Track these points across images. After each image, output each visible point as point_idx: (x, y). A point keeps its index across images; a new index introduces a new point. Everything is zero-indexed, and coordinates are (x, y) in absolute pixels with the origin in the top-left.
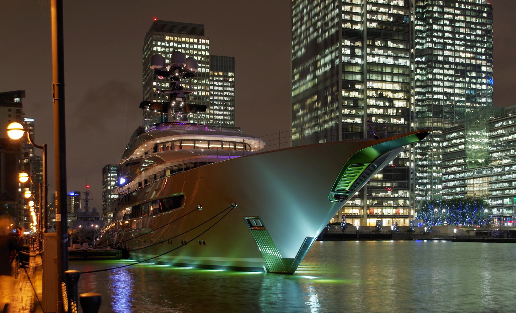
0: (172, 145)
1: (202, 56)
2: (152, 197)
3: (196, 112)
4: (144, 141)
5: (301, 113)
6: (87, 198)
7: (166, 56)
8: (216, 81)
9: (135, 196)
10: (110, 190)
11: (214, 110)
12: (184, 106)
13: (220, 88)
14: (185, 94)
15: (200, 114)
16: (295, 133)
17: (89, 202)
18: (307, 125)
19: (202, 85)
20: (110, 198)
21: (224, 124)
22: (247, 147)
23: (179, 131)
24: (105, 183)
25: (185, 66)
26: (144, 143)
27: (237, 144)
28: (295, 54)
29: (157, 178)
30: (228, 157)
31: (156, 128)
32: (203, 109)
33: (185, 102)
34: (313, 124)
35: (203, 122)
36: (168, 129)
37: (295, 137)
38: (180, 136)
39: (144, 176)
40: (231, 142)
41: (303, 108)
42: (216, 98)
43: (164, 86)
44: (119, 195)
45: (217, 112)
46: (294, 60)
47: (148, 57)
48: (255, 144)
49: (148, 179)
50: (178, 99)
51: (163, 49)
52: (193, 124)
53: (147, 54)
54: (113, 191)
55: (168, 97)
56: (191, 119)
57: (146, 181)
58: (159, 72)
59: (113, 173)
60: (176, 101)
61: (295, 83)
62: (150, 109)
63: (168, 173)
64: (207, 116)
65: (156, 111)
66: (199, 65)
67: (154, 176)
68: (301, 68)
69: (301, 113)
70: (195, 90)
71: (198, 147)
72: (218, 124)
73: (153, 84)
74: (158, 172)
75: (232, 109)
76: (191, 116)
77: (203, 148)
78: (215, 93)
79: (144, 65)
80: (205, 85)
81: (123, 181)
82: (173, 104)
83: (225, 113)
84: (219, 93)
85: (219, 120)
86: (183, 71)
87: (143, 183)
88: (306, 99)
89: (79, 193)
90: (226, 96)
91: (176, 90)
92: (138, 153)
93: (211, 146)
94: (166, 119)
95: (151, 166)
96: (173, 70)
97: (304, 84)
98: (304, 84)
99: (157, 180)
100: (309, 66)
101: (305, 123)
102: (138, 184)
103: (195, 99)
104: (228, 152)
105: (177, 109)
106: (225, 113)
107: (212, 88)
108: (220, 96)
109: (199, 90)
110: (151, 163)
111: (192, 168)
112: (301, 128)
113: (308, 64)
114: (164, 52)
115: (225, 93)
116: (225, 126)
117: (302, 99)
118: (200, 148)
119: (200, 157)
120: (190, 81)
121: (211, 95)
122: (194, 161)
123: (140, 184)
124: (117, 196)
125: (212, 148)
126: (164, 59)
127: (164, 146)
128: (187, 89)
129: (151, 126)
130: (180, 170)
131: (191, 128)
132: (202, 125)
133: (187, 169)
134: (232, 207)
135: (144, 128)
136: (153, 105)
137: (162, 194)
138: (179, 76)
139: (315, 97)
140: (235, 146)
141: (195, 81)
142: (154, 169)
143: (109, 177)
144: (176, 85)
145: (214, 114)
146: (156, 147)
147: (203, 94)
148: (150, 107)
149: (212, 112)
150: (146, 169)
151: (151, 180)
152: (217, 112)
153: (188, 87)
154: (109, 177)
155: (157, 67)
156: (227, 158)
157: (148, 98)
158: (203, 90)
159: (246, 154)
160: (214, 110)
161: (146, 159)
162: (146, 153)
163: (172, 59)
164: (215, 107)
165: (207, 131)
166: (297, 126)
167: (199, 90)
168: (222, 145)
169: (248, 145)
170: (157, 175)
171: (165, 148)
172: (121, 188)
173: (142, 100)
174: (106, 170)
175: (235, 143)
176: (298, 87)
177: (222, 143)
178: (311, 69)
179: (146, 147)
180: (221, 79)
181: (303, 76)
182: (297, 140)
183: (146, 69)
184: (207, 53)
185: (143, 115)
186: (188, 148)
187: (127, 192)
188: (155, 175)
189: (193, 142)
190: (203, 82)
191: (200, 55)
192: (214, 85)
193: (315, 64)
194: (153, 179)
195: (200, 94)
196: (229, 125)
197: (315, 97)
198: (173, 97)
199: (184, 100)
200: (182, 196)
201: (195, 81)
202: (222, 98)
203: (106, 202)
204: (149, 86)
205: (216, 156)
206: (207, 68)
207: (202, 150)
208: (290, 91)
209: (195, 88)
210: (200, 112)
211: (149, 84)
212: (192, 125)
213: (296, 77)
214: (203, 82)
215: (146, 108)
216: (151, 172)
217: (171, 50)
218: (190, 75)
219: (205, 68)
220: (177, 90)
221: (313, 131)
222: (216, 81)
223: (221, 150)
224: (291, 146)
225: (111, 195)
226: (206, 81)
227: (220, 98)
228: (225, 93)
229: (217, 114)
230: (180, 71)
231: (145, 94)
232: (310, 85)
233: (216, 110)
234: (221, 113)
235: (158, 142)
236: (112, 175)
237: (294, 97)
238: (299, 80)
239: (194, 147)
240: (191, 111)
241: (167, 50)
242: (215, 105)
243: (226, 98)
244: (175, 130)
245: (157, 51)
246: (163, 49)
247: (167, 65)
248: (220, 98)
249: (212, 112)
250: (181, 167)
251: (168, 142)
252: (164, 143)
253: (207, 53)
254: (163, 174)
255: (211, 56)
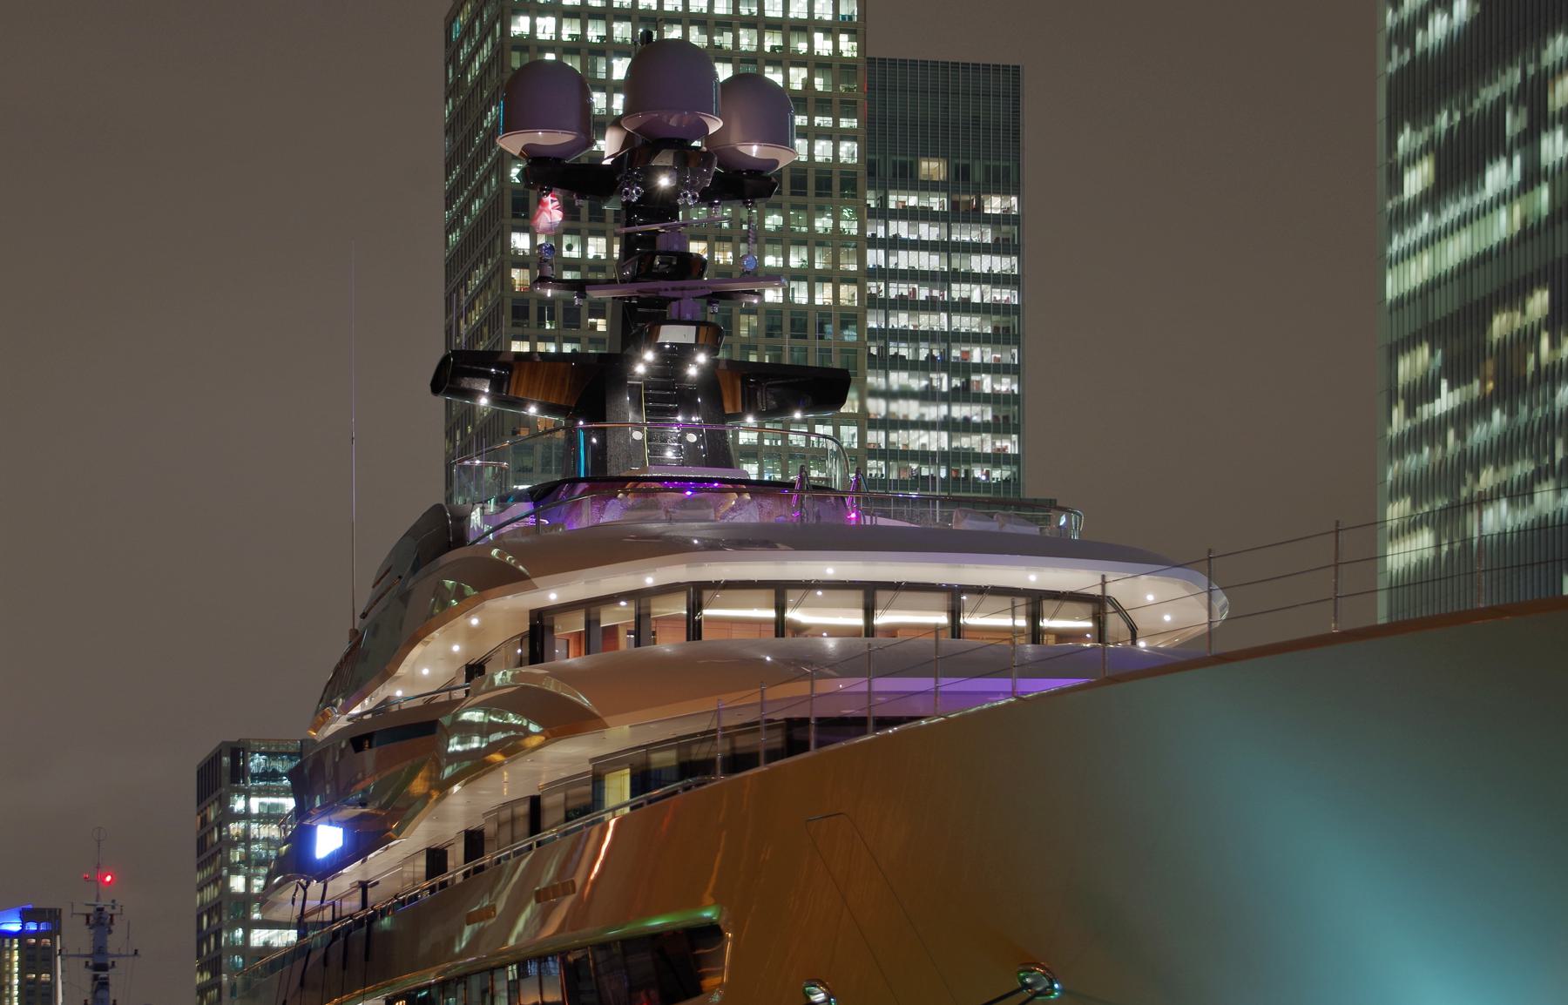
0: (641, 618)
1: (814, 63)
2: (512, 941)
3: (783, 409)
4: (460, 595)
5: (1446, 401)
6: (100, 950)
7: (589, 68)
8: (906, 214)
9: (387, 934)
10: (246, 900)
11: (889, 395)
12: (711, 383)
13: (930, 262)
14: (718, 300)
15: (804, 422)
16: (1411, 526)
17: (113, 976)
18: (1488, 478)
19: (812, 241)
20: (245, 949)
21: (952, 482)
22: (1114, 623)
23: (679, 529)
24: (211, 852)
25: (715, 126)
26: (468, 606)
27: (1048, 606)
28: (1404, 35)
29: (548, 819)
30: (1004, 684)
31: (536, 514)
32: (823, 389)
33: (713, 350)
34: (1523, 468)
35: (835, 473)
36: (607, 518)
37: (1410, 551)
38: (689, 563)
39: (458, 809)
40: (998, 590)
41: (1457, 372)
42: (901, 320)
43: (575, 253)
44: (301, 925)
45: (910, 409)
46: (1401, 70)
47: (480, 81)
48: (1164, 607)
49: (490, 829)
50: (671, 335)
51: (570, 29)
52: (760, 483)
53: (471, 58)
54: (263, 899)
55: (601, 325)
56: (751, 453)
57: (474, 841)
58: (547, 171)
59: (261, 792)
60: (660, 348)
61: (1405, 216)
62: (496, 397)
63: (619, 788)
64: (849, 433)
65: (532, 410)
66: (800, 120)
67: (524, 809)
68: (1443, 121)
69: (1446, 401)
70: (773, 277)
71: (799, 629)
72: (920, 481)
73: (506, 243)
74: (553, 786)
75: (1006, 385)
76: (745, 438)
77: (834, 631)
78: (897, 290)
79: (450, 129)
80: (835, 240)
81: (328, 839)
82: (644, 363)
83: (959, 411)
84: (923, 293)
85: (924, 456)
86: (705, 158)
87: (456, 855)
88: (1480, 313)
89: (49, 917)
90: (965, 307)
91: (658, 279)
92: (426, 668)
93: (882, 619)
94: (599, 455)
95: (513, 747)
96: (638, 153)
97: (1464, 221)
98: (1464, 221)
99: (547, 835)
100: (1498, 108)
101: (1470, 463)
102: (422, 863)
103: (772, 329)
104: (994, 658)
105: (667, 394)
106: (959, 411)
107: (875, 257)
108: (931, 306)
109: (798, 275)
110: (511, 727)
111: (773, 755)
112: (1447, 499)
113: (1489, 94)
114: (579, 46)
115: (959, 291)
116: (961, 493)
117: (1455, 318)
118: (819, 630)
119: (824, 686)
120: (735, 222)
121: (874, 303)
122: (779, 716)
123: (436, 859)
124: (291, 936)
125: (892, 631)
126: (584, 85)
127: (591, 623)
128: (725, 273)
129: (503, 501)
130: (691, 769)
131: (747, 513)
132: (822, 489)
133: (738, 762)
134: (1026, 993)
135: (462, 519)
136: (510, 376)
137: (575, 919)
138: (675, 193)
139: (1539, 302)
140: (1034, 617)
141: (773, 221)
142: (525, 765)
143: (238, 817)
144: (661, 244)
145: (890, 424)
146: (538, 634)
147: (824, 295)
148: (497, 385)
149: (877, 407)
150: (476, 766)
151: (506, 834)
152: (910, 409)
153: (725, 257)
154: (238, 817)
155: (541, 138)
156: (998, 693)
157: (475, 334)
158: (823, 277)
159: (1113, 670)
160: (889, 395)
161: (475, 707)
162: (475, 670)
163: (630, 86)
164: (898, 379)
165: (860, 528)
166: (1415, 488)
167: (798, 275)
168: (955, 613)
169: (1119, 610)
170: (547, 802)
171: (597, 638)
172: (315, 887)
173: (439, 352)
174: (220, 775)
175: (1036, 601)
176: (1428, 242)
177: (954, 597)
178: (1513, 124)
179: (473, 634)
180: (936, 202)
181: (1459, 166)
182: (1420, 578)
183: (467, 151)
184: (848, 47)
185: (450, 435)
186: (738, 634)
187: (352, 904)
188: (535, 802)
189: (770, 595)
190: (823, 223)
191: (799, 61)
192: (893, 244)
193: (1534, 94)
194: (523, 827)
195: (801, 296)
196: (987, 486)
197: (1539, 302)
198: (638, 322)
199: (713, 335)
200: (711, 932)
201: (773, 221)
202: (937, 322)
203: (216, 973)
204: (482, 259)
205: (926, 684)
206: (848, 135)
207: (831, 644)
208: (1380, 264)
209: (770, 261)
210: (806, 410)
211: (480, 245)
212: (760, 488)
213: (1416, 180)
214: (823, 223)
215: (473, 394)
216: (508, 784)
217: (622, 31)
218: (745, 185)
219: (836, 135)
220: (662, 276)
221: (1524, 516)
222: (906, 214)
223: (945, 638)
224: (1382, 619)
225: (249, 926)
226: (837, 219)
227: (926, 321)
228: (959, 291)
229: (907, 419)
230: (686, 160)
231: (453, 306)
232: (1503, 225)
233: (906, 394)
234: (935, 412)
235: (553, 597)
236: (255, 804)
237: (1400, 302)
238: (1432, 198)
239: (781, 627)
240: (749, 405)
241: (595, 32)
242: (899, 363)
243: (964, 323)
244: (655, 527)
245: (529, 44)
246: (570, 29)
247: (601, 125)
248: (926, 321)
249: (877, 407)
250: (699, 753)
251: (612, 599)
252: (591, 606)
253: (848, 47)
254: (585, 803)
255: (871, 61)
